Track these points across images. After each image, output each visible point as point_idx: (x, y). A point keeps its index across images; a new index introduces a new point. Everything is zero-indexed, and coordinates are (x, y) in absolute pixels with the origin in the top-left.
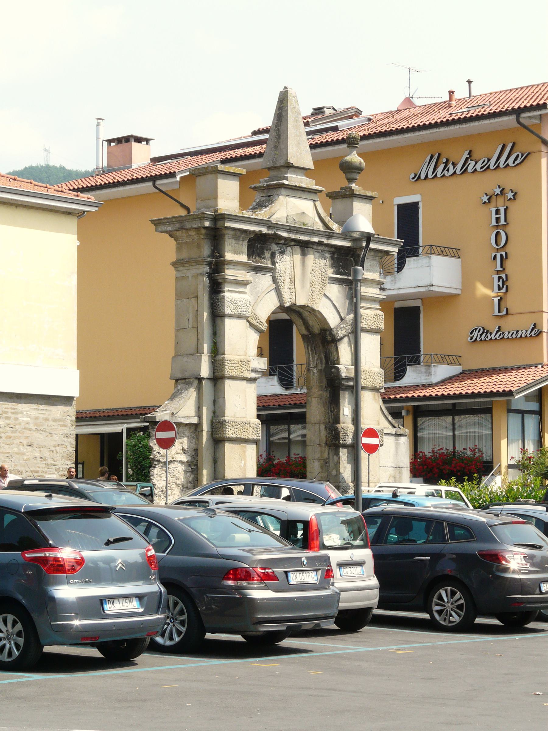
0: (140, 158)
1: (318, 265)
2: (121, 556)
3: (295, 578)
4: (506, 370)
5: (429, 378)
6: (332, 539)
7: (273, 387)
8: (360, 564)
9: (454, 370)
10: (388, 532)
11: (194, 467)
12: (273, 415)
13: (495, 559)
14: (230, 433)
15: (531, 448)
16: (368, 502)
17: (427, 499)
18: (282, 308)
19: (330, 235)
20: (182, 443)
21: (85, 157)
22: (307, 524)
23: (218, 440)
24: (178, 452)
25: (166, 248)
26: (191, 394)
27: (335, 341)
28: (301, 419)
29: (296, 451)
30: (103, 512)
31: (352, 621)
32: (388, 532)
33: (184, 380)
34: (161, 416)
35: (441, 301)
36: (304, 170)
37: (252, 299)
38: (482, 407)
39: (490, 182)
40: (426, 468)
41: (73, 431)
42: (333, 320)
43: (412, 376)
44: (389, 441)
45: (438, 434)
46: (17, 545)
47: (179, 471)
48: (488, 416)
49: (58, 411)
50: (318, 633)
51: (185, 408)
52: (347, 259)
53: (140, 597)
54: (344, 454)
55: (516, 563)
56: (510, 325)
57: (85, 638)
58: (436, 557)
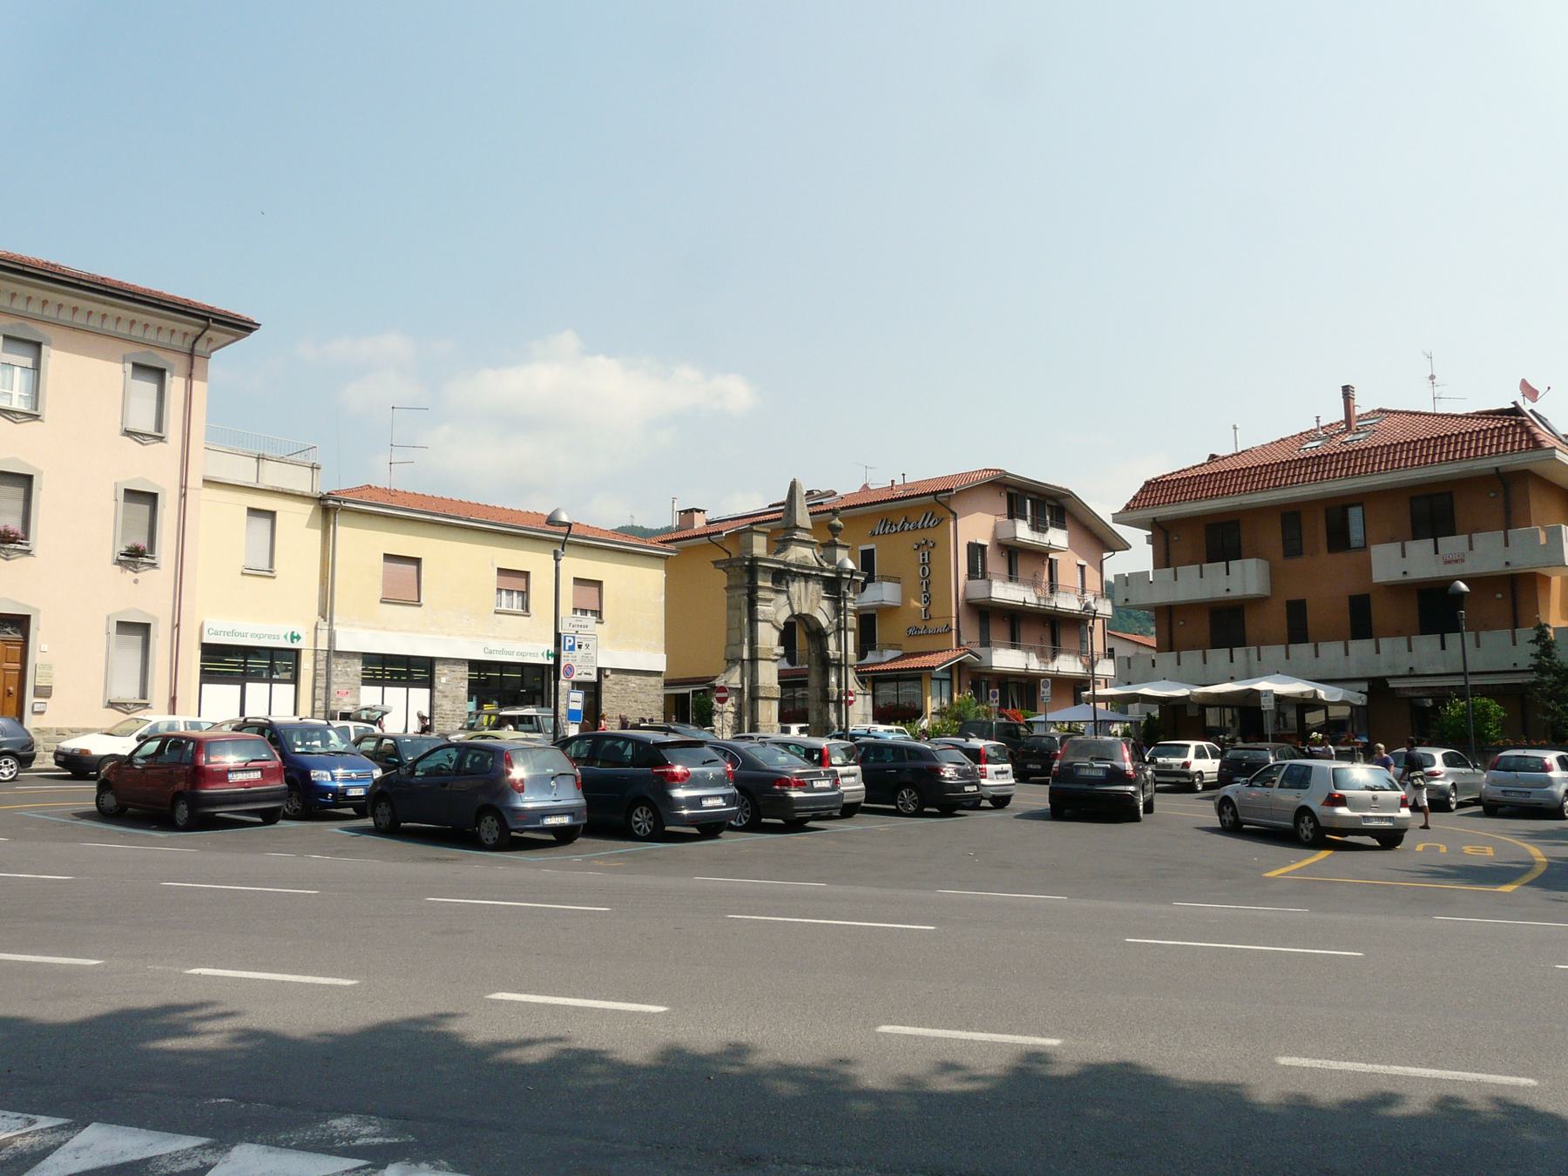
0: (699, 522)
1: (815, 588)
2: (711, 771)
3: (817, 784)
4: (930, 653)
5: (884, 658)
6: (836, 760)
7: (786, 665)
8: (854, 775)
9: (899, 653)
10: (868, 754)
11: (739, 715)
12: (786, 681)
13: (937, 770)
14: (762, 694)
15: (945, 701)
16: (853, 737)
17: (888, 733)
18: (793, 615)
19: (823, 570)
20: (732, 700)
21: (663, 519)
22: (820, 751)
23: (754, 698)
24: (729, 706)
25: (721, 578)
26: (738, 669)
27: (826, 636)
28: (804, 684)
29: (799, 705)
30: (700, 744)
31: (849, 810)
32: (868, 754)
33: (733, 660)
34: (719, 683)
35: (887, 610)
36: (806, 530)
37: (774, 610)
38: (916, 676)
39: (919, 537)
40: (882, 715)
41: (662, 692)
42: (824, 623)
43: (871, 657)
44: (860, 698)
45: (888, 692)
46: (1420, 750)
47: (730, 717)
48: (208, 639)
49: (653, 680)
50: (830, 818)
51: (734, 679)
52: (834, 586)
53: (723, 796)
54: (832, 707)
55: (949, 772)
56: (932, 625)
57: (691, 821)
58: (900, 770)
